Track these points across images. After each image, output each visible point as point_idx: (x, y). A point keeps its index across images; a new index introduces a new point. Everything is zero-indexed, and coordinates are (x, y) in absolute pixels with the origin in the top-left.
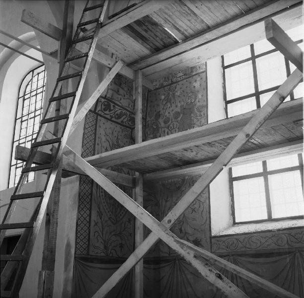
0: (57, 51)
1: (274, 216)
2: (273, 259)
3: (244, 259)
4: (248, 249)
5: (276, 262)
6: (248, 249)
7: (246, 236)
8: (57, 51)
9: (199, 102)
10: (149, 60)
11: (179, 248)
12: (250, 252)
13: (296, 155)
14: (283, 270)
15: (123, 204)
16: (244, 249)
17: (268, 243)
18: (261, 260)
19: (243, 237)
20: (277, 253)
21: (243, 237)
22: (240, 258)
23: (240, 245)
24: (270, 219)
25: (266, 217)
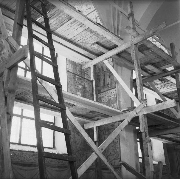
0: (130, 47)
1: (22, 143)
2: (32, 168)
3: (16, 166)
4: (19, 161)
5: (33, 170)
6: (19, 161)
7: (20, 152)
8: (130, 47)
9: (4, 54)
10: (9, 12)
11: (108, 164)
12: (21, 163)
13: (21, 109)
14: (35, 175)
15: (80, 131)
16: (17, 160)
17: (30, 159)
18: (25, 168)
19: (18, 152)
20: (34, 165)
21: (18, 152)
22: (14, 165)
23: (16, 157)
24: (20, 144)
25: (18, 142)
